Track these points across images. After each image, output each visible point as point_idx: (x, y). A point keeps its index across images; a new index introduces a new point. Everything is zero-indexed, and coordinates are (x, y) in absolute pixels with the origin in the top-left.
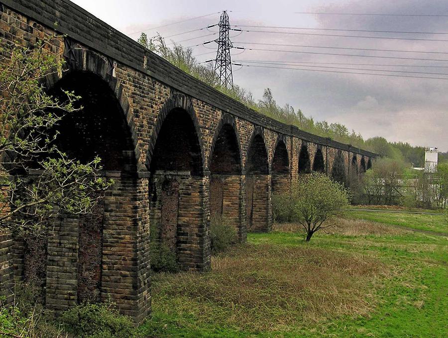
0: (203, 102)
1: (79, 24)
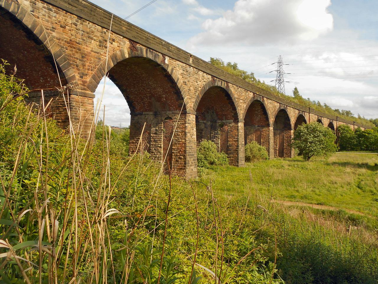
0: (237, 86)
1: (139, 35)
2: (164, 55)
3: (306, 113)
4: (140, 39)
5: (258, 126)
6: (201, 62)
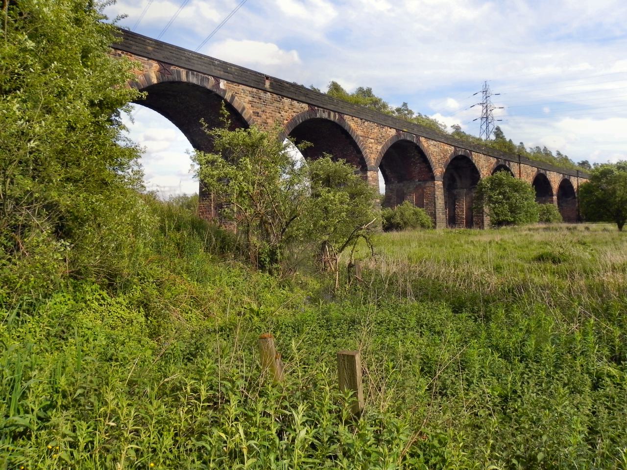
0: (361, 119)
1: (174, 55)
2: (217, 78)
3: (512, 164)
4: (175, 59)
5: (419, 181)
6: (288, 85)
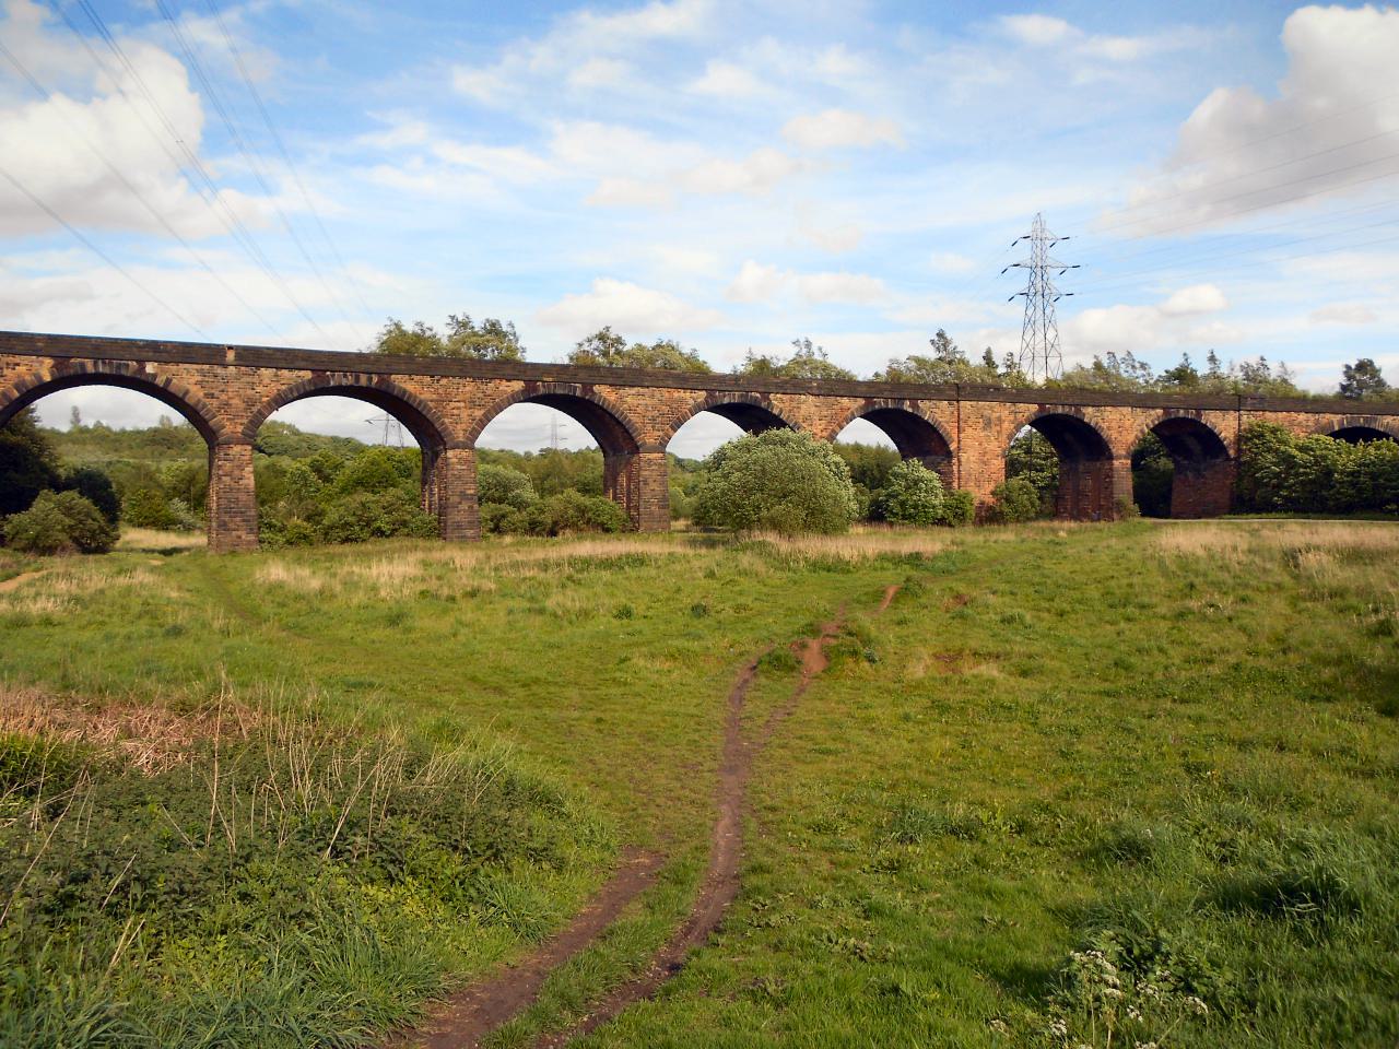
2: (141, 362)
